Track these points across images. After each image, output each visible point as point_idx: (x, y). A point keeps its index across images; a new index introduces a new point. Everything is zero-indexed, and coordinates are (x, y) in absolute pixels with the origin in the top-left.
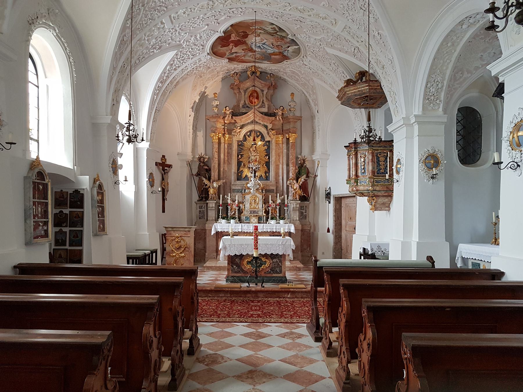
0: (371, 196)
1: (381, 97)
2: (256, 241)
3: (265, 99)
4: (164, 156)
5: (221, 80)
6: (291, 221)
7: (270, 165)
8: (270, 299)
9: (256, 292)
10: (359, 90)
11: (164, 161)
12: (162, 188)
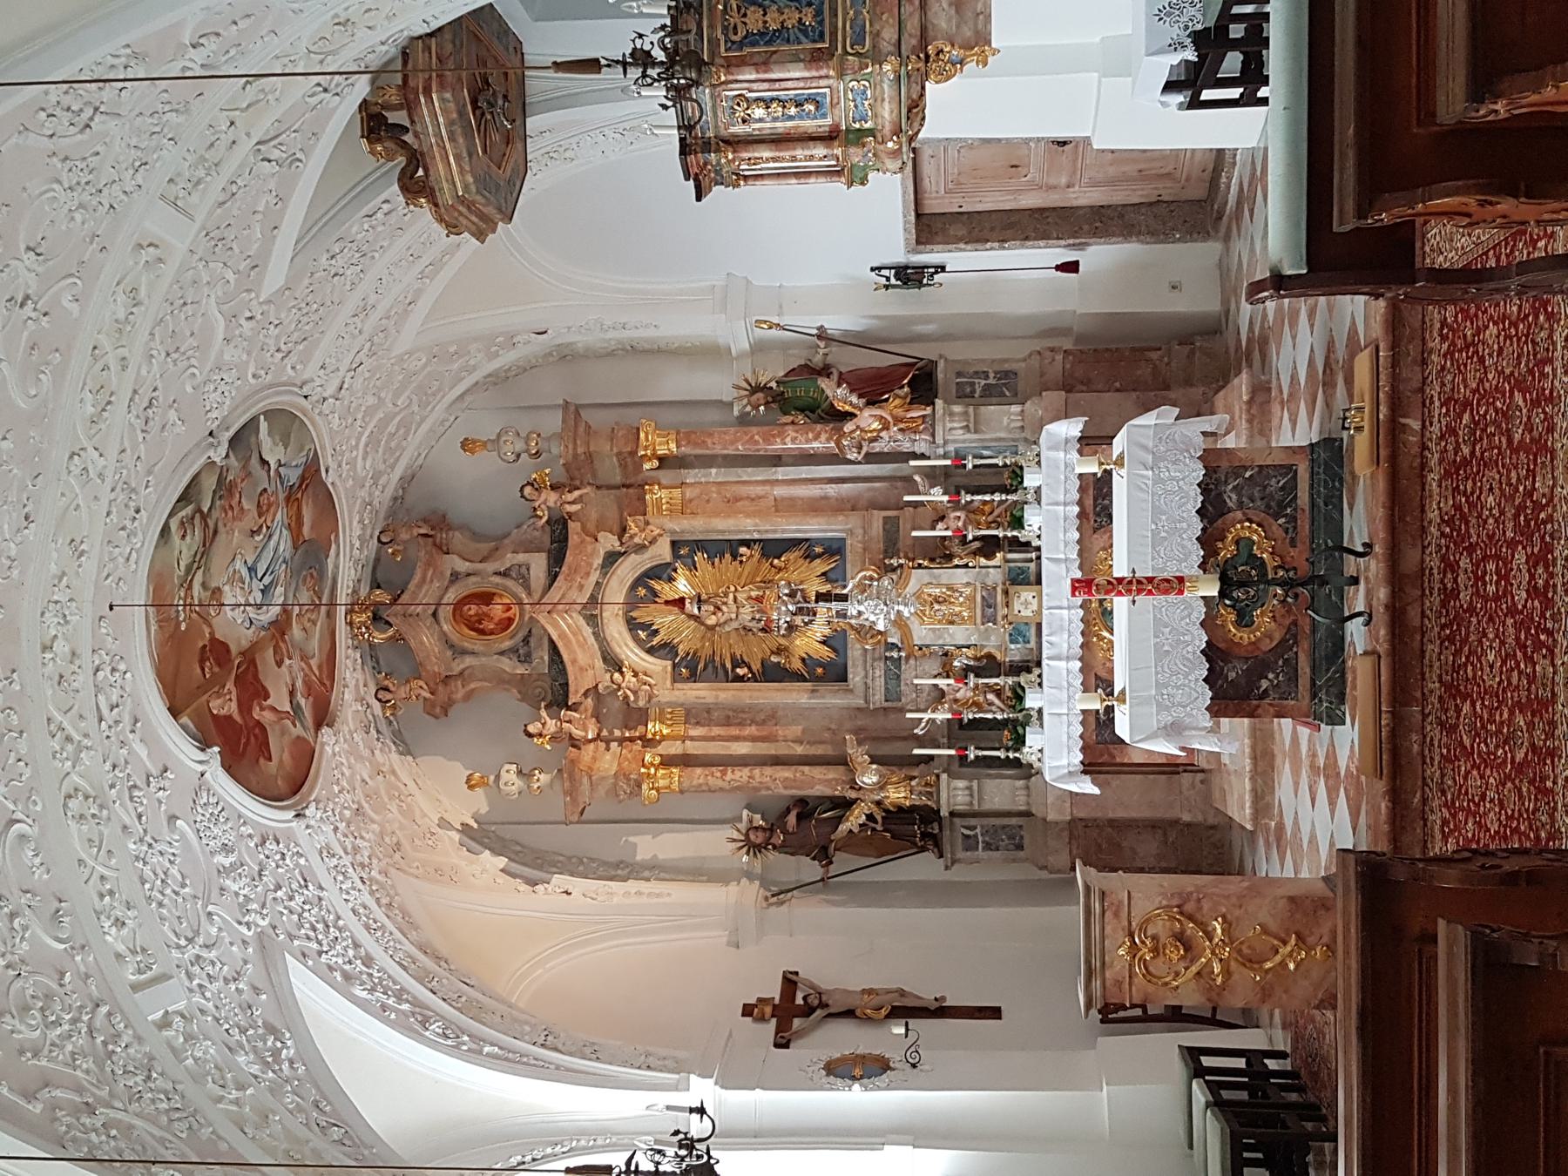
0: (921, 65)
1: (476, 35)
2: (1136, 585)
3: (490, 567)
4: (748, 1011)
5: (410, 758)
6: (1026, 440)
7: (778, 536)
8: (1433, 515)
9: (1396, 578)
10: (446, 139)
11: (768, 1010)
12: (887, 1017)
